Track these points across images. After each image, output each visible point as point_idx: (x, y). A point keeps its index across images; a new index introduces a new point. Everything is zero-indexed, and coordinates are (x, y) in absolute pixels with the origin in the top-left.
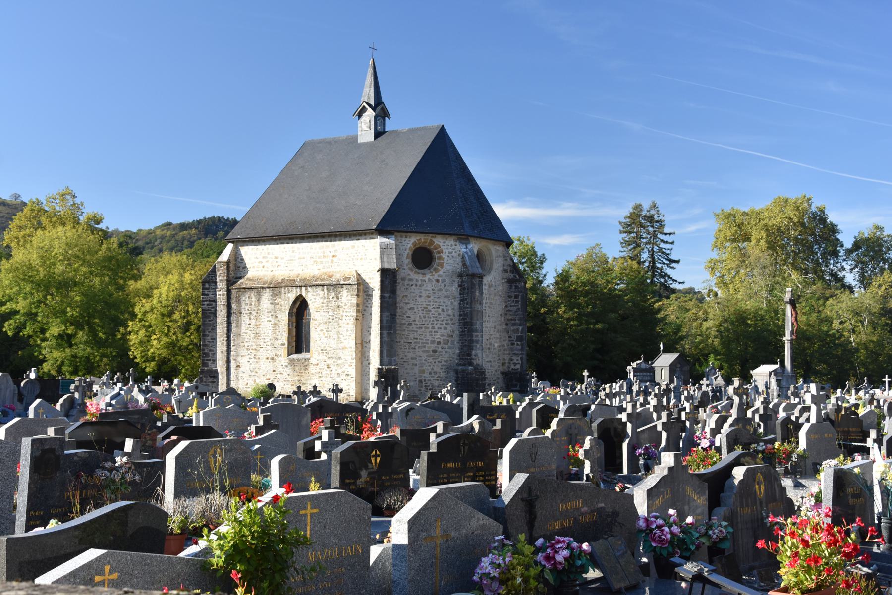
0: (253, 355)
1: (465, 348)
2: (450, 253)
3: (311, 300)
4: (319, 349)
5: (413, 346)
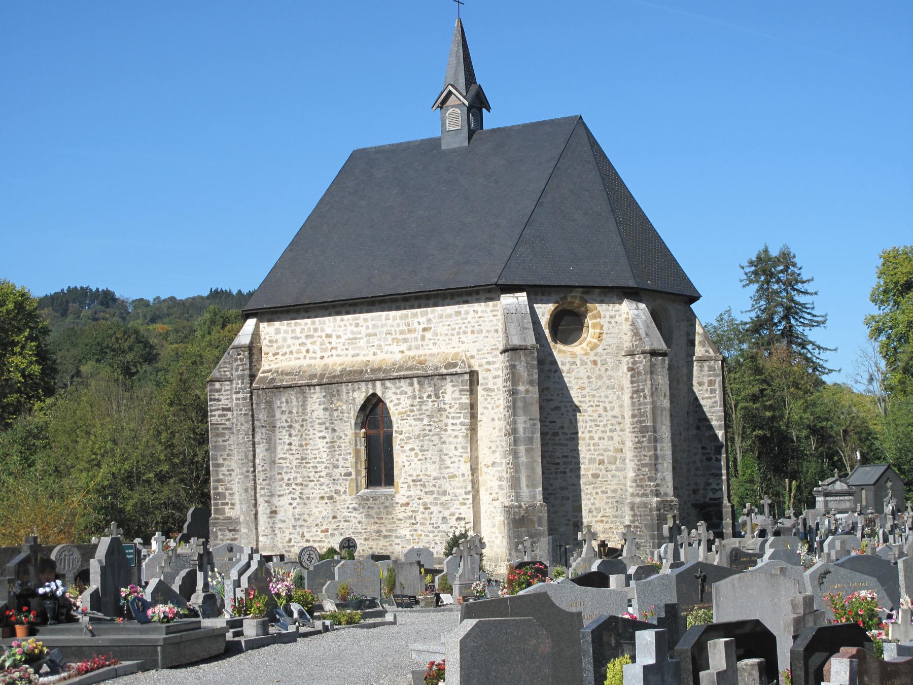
0: (297, 494)
1: (644, 469)
3: (391, 401)
4: (410, 479)
5: (562, 468)
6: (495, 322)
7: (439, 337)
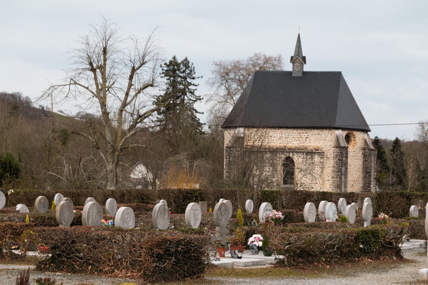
2: (359, 138)
6: (331, 138)
7: (311, 140)
